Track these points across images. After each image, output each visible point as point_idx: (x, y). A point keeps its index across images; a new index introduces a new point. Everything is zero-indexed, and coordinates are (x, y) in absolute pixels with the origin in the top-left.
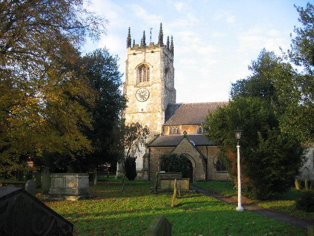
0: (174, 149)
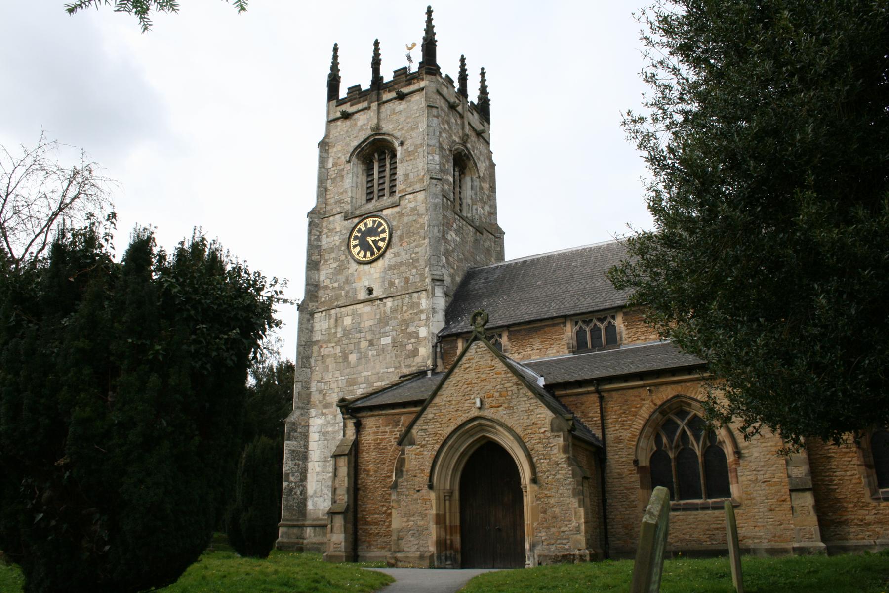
0: (419, 415)
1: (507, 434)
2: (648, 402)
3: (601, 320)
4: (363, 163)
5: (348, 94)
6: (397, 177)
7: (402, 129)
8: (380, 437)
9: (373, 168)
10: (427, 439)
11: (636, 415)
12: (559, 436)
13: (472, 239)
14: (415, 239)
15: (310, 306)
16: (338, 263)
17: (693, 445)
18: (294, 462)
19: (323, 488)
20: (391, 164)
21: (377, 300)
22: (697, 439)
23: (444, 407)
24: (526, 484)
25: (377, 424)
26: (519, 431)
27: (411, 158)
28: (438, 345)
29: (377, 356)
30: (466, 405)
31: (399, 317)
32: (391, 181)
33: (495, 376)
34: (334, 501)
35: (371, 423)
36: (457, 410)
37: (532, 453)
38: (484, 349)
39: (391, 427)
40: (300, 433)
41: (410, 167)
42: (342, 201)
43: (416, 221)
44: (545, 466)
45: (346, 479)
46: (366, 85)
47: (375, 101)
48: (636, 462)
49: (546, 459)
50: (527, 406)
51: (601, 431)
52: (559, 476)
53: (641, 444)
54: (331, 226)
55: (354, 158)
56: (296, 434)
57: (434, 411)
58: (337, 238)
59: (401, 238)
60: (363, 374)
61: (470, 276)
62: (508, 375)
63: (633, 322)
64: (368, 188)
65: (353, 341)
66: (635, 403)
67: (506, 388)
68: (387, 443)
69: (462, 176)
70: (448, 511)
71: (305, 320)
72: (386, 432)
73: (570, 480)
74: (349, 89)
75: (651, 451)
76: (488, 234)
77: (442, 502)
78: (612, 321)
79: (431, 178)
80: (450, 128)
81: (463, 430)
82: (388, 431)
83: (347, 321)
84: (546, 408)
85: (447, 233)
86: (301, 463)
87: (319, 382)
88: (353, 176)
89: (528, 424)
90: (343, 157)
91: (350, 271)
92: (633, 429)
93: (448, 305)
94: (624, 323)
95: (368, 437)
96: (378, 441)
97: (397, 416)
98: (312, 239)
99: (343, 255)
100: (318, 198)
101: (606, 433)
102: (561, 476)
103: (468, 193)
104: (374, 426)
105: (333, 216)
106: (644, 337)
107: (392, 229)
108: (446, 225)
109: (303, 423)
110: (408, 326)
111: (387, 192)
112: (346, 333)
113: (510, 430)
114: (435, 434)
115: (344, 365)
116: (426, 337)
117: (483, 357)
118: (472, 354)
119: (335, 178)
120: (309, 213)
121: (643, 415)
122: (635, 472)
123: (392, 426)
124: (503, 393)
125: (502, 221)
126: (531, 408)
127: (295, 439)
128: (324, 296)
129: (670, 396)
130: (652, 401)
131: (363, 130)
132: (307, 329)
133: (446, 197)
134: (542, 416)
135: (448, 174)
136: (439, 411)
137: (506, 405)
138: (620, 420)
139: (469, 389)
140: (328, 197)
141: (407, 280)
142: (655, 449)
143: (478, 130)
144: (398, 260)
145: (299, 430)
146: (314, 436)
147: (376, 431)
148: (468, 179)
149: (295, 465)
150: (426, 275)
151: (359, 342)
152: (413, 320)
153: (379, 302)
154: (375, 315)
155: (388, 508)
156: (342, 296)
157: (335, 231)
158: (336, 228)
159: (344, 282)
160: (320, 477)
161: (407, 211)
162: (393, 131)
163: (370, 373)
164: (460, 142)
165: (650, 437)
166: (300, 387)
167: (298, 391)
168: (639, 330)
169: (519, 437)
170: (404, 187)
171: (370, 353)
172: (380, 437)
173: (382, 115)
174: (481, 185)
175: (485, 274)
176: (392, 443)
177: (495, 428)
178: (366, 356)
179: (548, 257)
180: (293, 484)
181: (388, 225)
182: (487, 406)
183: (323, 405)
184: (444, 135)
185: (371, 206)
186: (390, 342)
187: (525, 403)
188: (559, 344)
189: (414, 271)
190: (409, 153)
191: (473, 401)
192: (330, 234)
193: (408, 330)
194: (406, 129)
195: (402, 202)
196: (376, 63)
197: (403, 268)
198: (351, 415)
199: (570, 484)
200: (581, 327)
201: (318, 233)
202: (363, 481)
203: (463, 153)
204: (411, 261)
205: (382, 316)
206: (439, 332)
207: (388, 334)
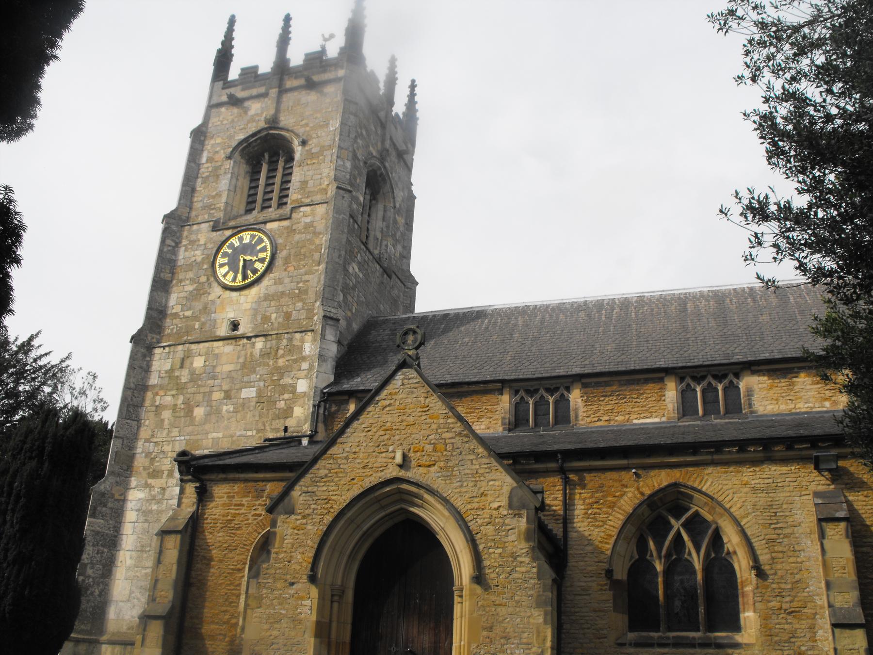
1: (439, 506)
2: (632, 490)
3: (551, 391)
4: (248, 162)
5: (240, 75)
6: (290, 185)
7: (307, 125)
8: (232, 511)
9: (260, 172)
10: (313, 506)
11: (614, 507)
12: (520, 515)
13: (378, 281)
14: (306, 264)
15: (149, 338)
16: (195, 285)
17: (690, 554)
18: (96, 548)
19: (134, 588)
20: (284, 169)
21: (244, 337)
22: (698, 549)
23: (344, 461)
24: (462, 584)
25: (229, 493)
26: (458, 503)
27: (314, 161)
28: (322, 403)
29: (233, 412)
30: (379, 460)
31: (271, 363)
32: (282, 190)
33: (428, 420)
34: (152, 599)
35: (221, 492)
36: (364, 468)
37: (478, 537)
38: (415, 381)
39: (250, 499)
40: (111, 508)
41: (311, 173)
42: (213, 207)
43: (311, 241)
44: (495, 559)
45: (175, 567)
46: (266, 66)
47: (275, 88)
48: (609, 573)
49: (498, 548)
50: (474, 467)
51: (561, 525)
52: (515, 575)
53: (618, 548)
54: (193, 237)
55: (237, 155)
56: (104, 509)
57: (329, 466)
58: (198, 253)
59: (287, 261)
60: (210, 436)
61: (370, 325)
62: (449, 421)
63: (595, 397)
64: (249, 196)
65: (202, 390)
66: (613, 490)
67: (445, 439)
68: (242, 521)
69: (373, 202)
70: (335, 618)
71: (139, 355)
72: (243, 505)
73: (532, 581)
74: (242, 70)
75: (630, 560)
76: (397, 280)
77: (328, 603)
78: (565, 393)
79: (338, 188)
80: (369, 135)
81: (372, 496)
82: (246, 503)
83: (198, 363)
84: (504, 473)
85: (349, 264)
86: (106, 550)
87: (147, 441)
88: (232, 177)
89: (474, 495)
90: (222, 151)
91: (211, 297)
92: (607, 527)
93: (339, 356)
94: (581, 397)
95: (215, 510)
96: (229, 518)
97: (261, 484)
98: (165, 250)
99: (204, 275)
100: (180, 199)
101: (569, 529)
102: (520, 576)
103: (377, 224)
104: (226, 495)
105: (198, 224)
106: (607, 418)
107: (276, 247)
108: (351, 255)
109: (117, 497)
110: (281, 378)
111: (274, 203)
112: (195, 377)
113: (445, 501)
114: (328, 500)
115: (186, 422)
116: (305, 393)
117: (412, 392)
118: (397, 387)
119: (208, 177)
120: (165, 216)
121: (624, 507)
122: (607, 587)
123: (253, 497)
124: (438, 447)
125: (416, 268)
126: (481, 471)
127: (102, 516)
128: (171, 326)
129: (665, 484)
130: (638, 489)
131: (254, 121)
132: (141, 367)
133: (353, 218)
134: (497, 483)
135: (358, 190)
136: (337, 466)
137: (442, 464)
138: (590, 512)
139: (386, 437)
140: (195, 199)
141: (288, 316)
142: (637, 557)
143: (400, 149)
144: (280, 288)
145: (110, 505)
146: (130, 516)
147: (227, 502)
148: (380, 207)
149: (97, 553)
150: (316, 311)
151: (211, 392)
152: (289, 369)
153: (245, 341)
154: (238, 358)
155: (232, 616)
156: (195, 329)
157: (197, 243)
158: (199, 240)
159: (200, 310)
160: (131, 574)
161: (300, 226)
162: (293, 126)
163: (220, 435)
164: (378, 156)
165: (631, 539)
166: (120, 446)
167: (116, 449)
168: (602, 408)
169: (459, 513)
170: (300, 197)
171: (225, 408)
172: (232, 511)
173: (283, 107)
174: (395, 218)
175: (391, 325)
176: (250, 521)
177: (421, 498)
178: (218, 411)
179: (478, 312)
180: (91, 580)
181: (271, 243)
182: (413, 463)
183: (149, 473)
184: (360, 141)
185: (250, 218)
186: (254, 395)
187: (472, 463)
188: (490, 418)
189: (299, 305)
190: (311, 155)
191: (392, 455)
192: (190, 247)
193: (282, 382)
194: (311, 125)
195: (294, 215)
196: (284, 41)
197: (285, 300)
198: (193, 476)
199: (533, 588)
200: (522, 398)
201: (173, 244)
202: (200, 573)
203: (379, 173)
204: (297, 291)
205: (249, 360)
206: (325, 388)
207: (252, 384)
